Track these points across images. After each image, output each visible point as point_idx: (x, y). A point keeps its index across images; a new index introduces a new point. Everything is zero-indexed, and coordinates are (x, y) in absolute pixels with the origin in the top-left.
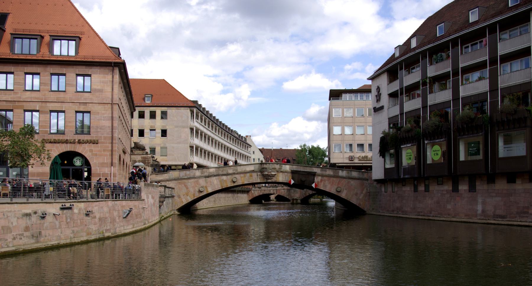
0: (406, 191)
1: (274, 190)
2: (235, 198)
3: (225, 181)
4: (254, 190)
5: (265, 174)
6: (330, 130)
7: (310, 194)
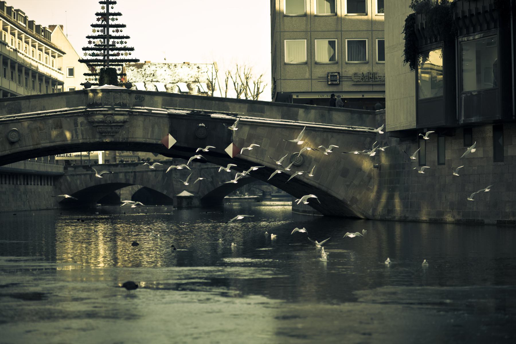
0: (474, 158)
1: (129, 172)
4: (73, 175)
5: (96, 120)
6: (275, 49)
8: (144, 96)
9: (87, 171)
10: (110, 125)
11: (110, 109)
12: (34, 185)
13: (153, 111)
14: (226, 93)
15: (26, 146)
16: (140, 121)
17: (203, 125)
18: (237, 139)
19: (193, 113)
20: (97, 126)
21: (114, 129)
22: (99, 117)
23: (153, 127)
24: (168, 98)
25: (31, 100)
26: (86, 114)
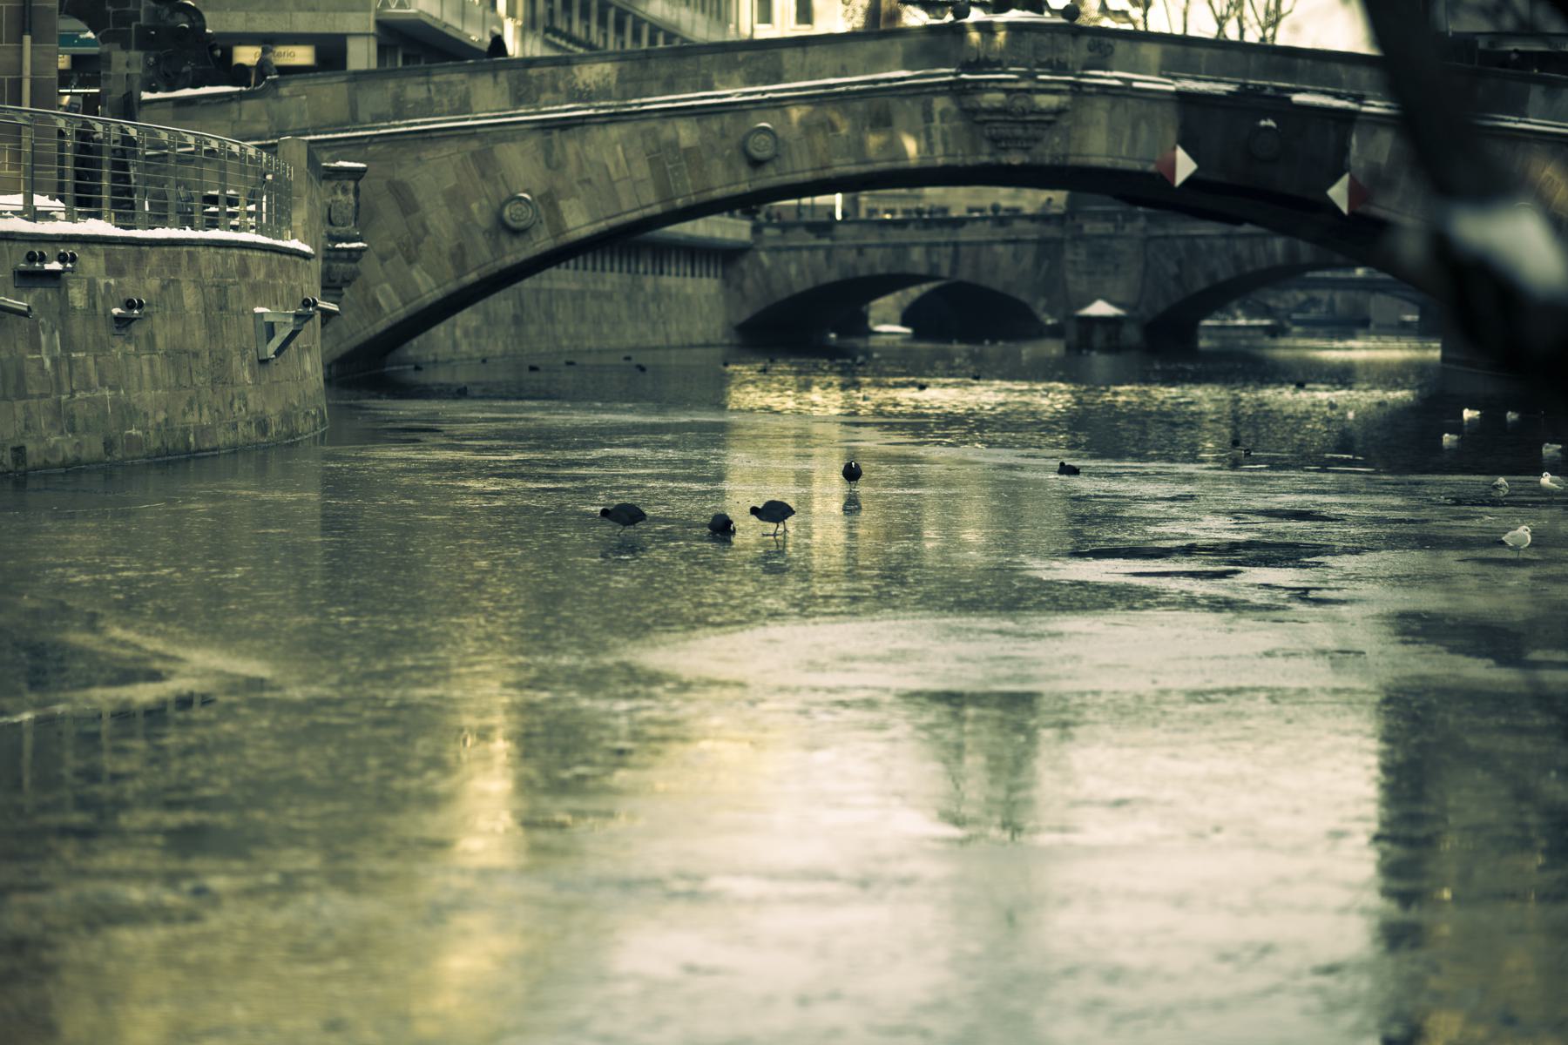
1: (938, 244)
2: (645, 306)
3: (687, 151)
4: (777, 250)
5: (984, 105)
7: (1222, 277)
8: (1111, 41)
9: (819, 237)
10: (1021, 119)
11: (1023, 76)
12: (677, 275)
13: (1136, 85)
14: (1185, 14)
15: (794, 172)
16: (1101, 107)
17: (1271, 123)
18: (1362, 165)
19: (1244, 93)
20: (985, 122)
21: (1031, 131)
22: (995, 98)
23: (1135, 127)
24: (1176, 49)
25: (809, 49)
26: (956, 90)
